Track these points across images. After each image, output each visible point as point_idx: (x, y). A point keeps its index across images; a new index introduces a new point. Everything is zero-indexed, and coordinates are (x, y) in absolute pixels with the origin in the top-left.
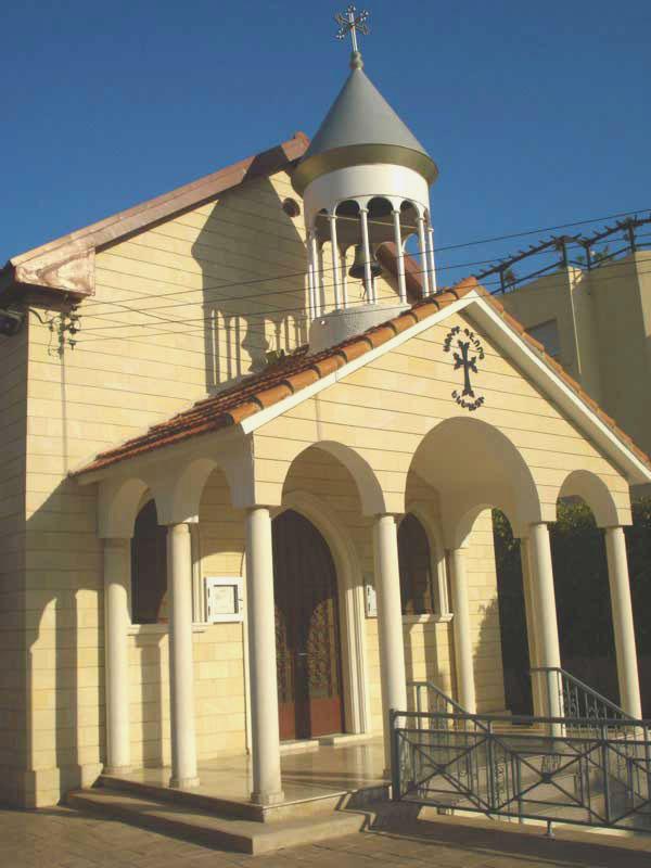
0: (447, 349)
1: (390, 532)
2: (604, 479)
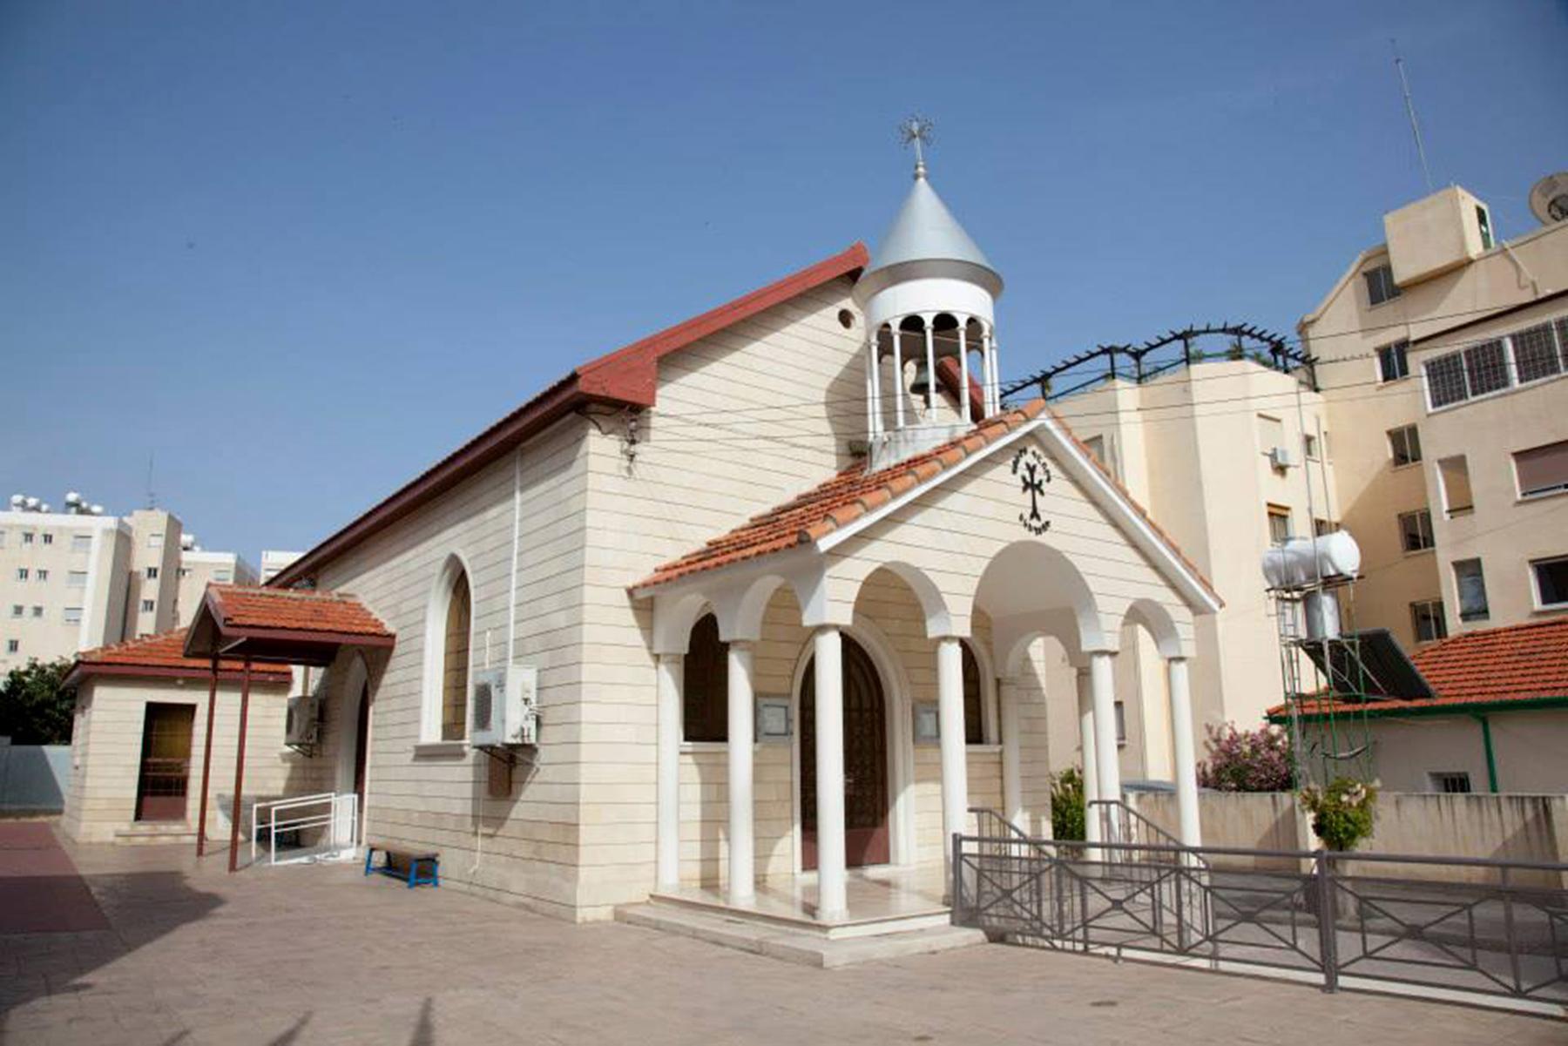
0: (1014, 472)
1: (951, 662)
2: (1168, 609)
